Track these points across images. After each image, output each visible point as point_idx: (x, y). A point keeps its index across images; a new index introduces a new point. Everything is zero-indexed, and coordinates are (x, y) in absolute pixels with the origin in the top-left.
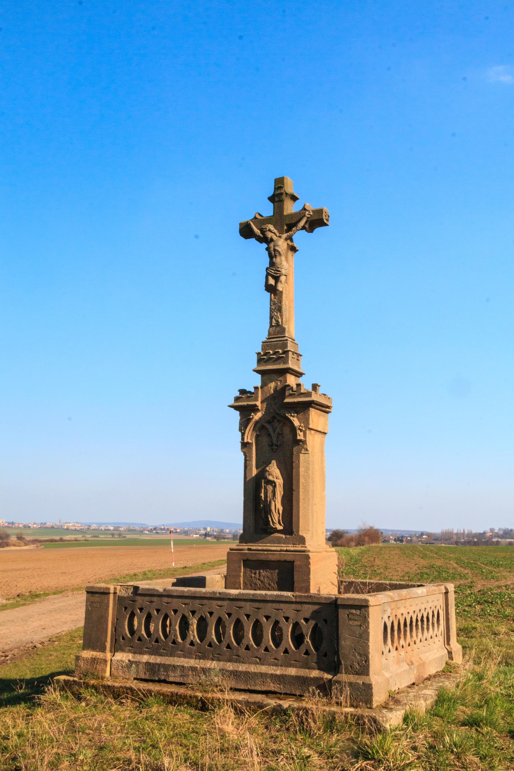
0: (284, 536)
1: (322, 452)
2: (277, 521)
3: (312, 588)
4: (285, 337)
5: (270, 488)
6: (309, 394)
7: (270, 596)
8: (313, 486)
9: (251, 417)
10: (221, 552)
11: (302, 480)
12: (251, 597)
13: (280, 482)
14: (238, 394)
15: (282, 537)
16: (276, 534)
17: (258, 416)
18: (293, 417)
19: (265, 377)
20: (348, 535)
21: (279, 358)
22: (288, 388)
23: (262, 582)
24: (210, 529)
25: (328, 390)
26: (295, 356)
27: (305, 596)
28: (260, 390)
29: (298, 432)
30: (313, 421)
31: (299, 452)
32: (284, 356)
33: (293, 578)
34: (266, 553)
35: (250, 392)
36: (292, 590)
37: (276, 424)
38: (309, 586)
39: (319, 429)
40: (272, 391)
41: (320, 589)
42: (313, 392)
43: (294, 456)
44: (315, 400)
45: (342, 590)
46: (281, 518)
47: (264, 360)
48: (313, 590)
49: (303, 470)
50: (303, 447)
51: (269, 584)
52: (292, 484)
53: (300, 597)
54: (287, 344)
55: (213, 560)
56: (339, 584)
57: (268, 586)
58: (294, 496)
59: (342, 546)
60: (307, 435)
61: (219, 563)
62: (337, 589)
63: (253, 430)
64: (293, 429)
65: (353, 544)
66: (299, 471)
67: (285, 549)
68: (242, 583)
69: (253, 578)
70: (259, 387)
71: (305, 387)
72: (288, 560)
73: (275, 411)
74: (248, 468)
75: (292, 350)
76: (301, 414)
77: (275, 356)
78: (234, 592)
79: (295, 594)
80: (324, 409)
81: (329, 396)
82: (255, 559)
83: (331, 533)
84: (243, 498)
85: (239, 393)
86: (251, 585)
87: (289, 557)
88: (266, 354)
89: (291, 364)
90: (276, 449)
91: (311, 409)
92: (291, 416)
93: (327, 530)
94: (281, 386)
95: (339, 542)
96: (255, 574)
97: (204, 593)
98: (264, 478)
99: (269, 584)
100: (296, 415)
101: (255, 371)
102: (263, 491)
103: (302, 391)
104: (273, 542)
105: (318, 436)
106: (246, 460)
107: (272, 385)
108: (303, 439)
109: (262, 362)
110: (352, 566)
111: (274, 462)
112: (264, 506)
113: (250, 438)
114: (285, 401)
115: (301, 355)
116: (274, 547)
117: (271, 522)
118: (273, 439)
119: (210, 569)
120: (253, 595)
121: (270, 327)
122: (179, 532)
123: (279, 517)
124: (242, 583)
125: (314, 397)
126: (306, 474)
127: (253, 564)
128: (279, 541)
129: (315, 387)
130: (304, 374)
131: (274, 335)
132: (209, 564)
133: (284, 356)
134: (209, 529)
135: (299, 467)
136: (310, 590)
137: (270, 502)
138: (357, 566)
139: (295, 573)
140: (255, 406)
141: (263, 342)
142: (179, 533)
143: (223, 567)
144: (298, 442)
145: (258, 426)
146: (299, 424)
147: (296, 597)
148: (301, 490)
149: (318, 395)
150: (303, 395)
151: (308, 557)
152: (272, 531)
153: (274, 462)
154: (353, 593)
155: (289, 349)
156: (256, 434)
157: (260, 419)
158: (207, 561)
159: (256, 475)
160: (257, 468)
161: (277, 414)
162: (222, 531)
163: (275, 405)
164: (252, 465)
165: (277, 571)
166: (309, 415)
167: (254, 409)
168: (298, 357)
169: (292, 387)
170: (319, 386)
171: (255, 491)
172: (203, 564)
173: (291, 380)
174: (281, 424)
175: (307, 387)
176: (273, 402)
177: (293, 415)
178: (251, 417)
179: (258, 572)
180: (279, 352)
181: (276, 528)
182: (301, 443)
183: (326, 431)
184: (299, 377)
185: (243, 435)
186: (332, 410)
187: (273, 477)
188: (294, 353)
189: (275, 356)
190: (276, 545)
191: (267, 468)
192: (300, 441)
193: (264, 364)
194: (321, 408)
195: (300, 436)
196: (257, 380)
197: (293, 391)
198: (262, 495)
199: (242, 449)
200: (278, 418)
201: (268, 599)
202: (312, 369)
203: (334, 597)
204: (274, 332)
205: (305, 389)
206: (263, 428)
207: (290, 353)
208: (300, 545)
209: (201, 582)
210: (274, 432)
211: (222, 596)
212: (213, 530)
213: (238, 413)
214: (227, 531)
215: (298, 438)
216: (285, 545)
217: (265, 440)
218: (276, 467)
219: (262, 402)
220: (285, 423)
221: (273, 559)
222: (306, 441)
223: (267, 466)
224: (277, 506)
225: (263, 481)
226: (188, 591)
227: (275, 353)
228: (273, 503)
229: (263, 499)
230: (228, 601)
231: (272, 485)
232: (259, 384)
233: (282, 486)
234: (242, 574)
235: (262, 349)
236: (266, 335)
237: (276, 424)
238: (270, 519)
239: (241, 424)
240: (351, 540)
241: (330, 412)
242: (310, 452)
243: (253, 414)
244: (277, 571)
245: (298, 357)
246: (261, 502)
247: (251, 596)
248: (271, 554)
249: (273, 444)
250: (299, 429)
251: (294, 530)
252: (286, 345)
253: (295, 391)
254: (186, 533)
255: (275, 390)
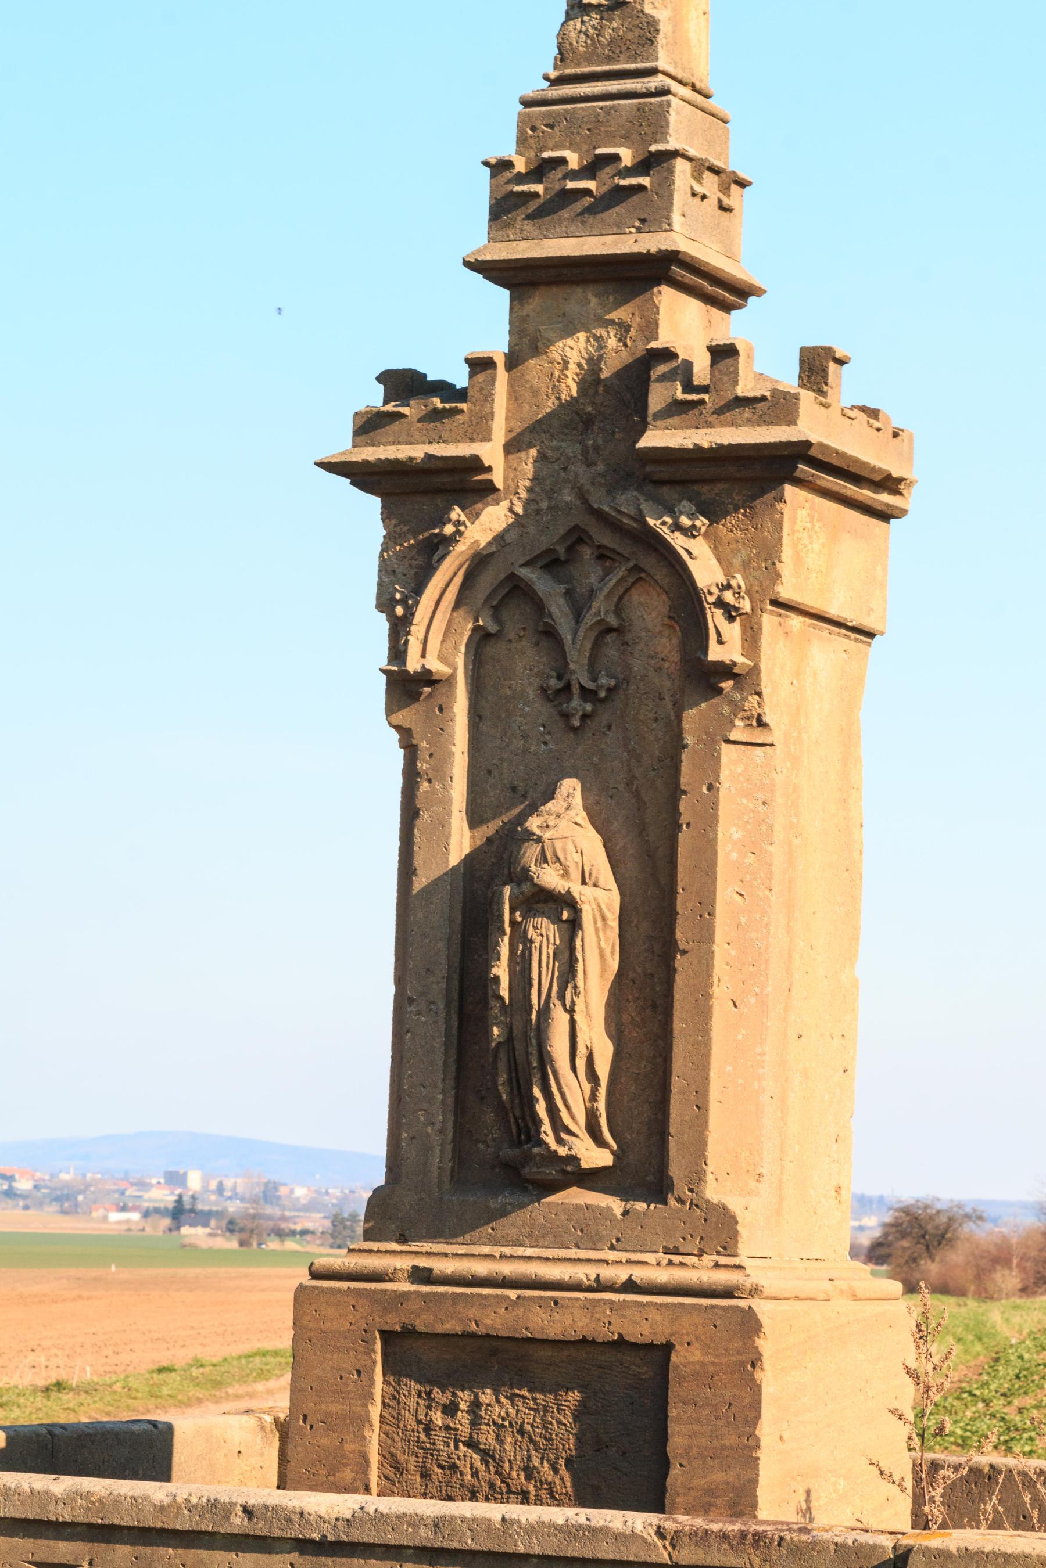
0: (616, 1205)
1: (848, 739)
2: (582, 1119)
3: (763, 1494)
4: (653, 72)
5: (544, 933)
6: (778, 406)
7: (531, 1530)
8: (789, 930)
9: (449, 529)
10: (259, 1310)
11: (725, 893)
12: (425, 1536)
13: (601, 901)
14: (374, 397)
15: (606, 1213)
16: (574, 1190)
17: (484, 526)
18: (690, 532)
19: (536, 301)
20: (981, 1233)
21: (619, 195)
22: (662, 369)
23: (486, 1455)
24: (205, 1180)
25: (895, 389)
26: (710, 184)
27: (725, 1537)
28: (502, 375)
29: (716, 618)
30: (798, 559)
31: (717, 736)
32: (645, 181)
33: (663, 1436)
34: (513, 1294)
35: (443, 389)
36: (655, 1500)
37: (588, 572)
38: (754, 1482)
39: (834, 611)
40: (571, 387)
41: (814, 1504)
42: (807, 397)
43: (685, 756)
44: (814, 438)
45: (935, 1511)
46: (601, 1106)
47: (533, 206)
48: (773, 1507)
49: (736, 836)
50: (737, 708)
51: (529, 1471)
52: (671, 914)
53: (702, 1538)
54: (662, 114)
55: (213, 1352)
56: (917, 1480)
57: (519, 1479)
58: (679, 980)
59: (943, 1289)
60: (765, 640)
61: (253, 1366)
62: (904, 1504)
63: (458, 604)
64: (688, 607)
65: (1009, 1279)
66: (711, 845)
67: (621, 1274)
68: (374, 1459)
69: (439, 1436)
70: (500, 361)
71: (758, 368)
72: (639, 1340)
73: (582, 495)
74: (425, 817)
75: (692, 152)
76: (731, 520)
77: (591, 185)
78: (326, 1506)
79: (669, 1525)
80: (869, 491)
81: (896, 423)
82: (451, 1326)
83: (888, 1218)
84: (389, 990)
85: (380, 388)
86: (425, 1475)
87: (643, 1322)
88: (540, 170)
89: (687, 231)
90: (585, 717)
91: (789, 490)
92: (677, 527)
93: (863, 1203)
94: (625, 357)
95: (932, 1268)
96: (450, 1410)
97: (161, 1509)
98: (510, 880)
99: (529, 1471)
100: (701, 522)
101: (475, 266)
102: (504, 949)
103: (741, 391)
104: (552, 1235)
105: (826, 650)
106: (411, 776)
107: (575, 349)
108: (739, 659)
109: (520, 215)
110: (998, 1404)
111: (570, 787)
112: (510, 1029)
113: (440, 644)
114: (642, 444)
115: (743, 184)
116: (559, 1265)
117: (546, 1126)
118: (572, 654)
119: (200, 1401)
120: (437, 1524)
121: (569, 17)
122: (24, 1196)
123: (594, 1097)
124: (374, 1459)
125: (813, 425)
126: (750, 859)
127: (436, 1357)
128: (587, 1232)
129: (817, 366)
130: (757, 291)
131: (589, 60)
132: (195, 1372)
133: (645, 181)
134: (194, 1182)
135: (711, 820)
136: (754, 1506)
137: (545, 1012)
138: (1029, 1401)
139: (673, 1413)
140: (475, 464)
141: (527, 103)
142: (29, 1201)
143: (270, 1392)
144: (708, 678)
145: (487, 581)
146: (721, 579)
147: (675, 1540)
148: (719, 948)
149: (835, 412)
150: (747, 413)
151: (749, 1325)
152: (552, 1173)
153: (570, 787)
154: (996, 1524)
155: (672, 144)
156: (476, 629)
157: (500, 539)
158: (181, 1357)
159: (470, 860)
160: (475, 819)
161: (599, 515)
162: (270, 1193)
163: (589, 464)
164: (446, 802)
165: (574, 1397)
166: (779, 526)
167: (466, 482)
168: (725, 189)
169: (688, 365)
170: (841, 362)
171: (459, 943)
172: (161, 1370)
173: (682, 324)
174: (621, 572)
175: (769, 362)
176: (572, 449)
177: (685, 521)
178: (449, 529)
179: (464, 1398)
180: (616, 158)
181: (574, 1159)
182: (727, 685)
183: (868, 622)
184: (727, 308)
185: (399, 629)
186: (912, 500)
187: (566, 875)
188: (702, 167)
189: (591, 185)
190: (573, 1253)
191: (534, 823)
192: (726, 670)
193: (529, 227)
194: (850, 489)
195: (726, 645)
196: (486, 319)
197: (689, 387)
198: (501, 970)
199: (390, 710)
200: (606, 539)
201: (521, 1549)
202: (813, 262)
203: (887, 1542)
204: (594, 42)
205: (760, 377)
206: (514, 589)
207: (681, 166)
208: (708, 1259)
209: (145, 1451)
210: (578, 617)
211: (260, 1528)
212: (220, 1189)
213: (374, 503)
214: (300, 1192)
215: (715, 653)
216: (623, 1256)
217: (524, 665)
218: (582, 817)
219: (512, 447)
220: (637, 568)
221: (554, 1332)
222: (755, 670)
223: (533, 809)
224: (583, 1033)
225: (507, 891)
226: (68, 1500)
227: (593, 167)
228: (560, 1020)
229: (504, 992)
230: (294, 1557)
231: (557, 920)
232: (497, 343)
233: (615, 924)
234: (375, 1411)
235: (522, 141)
236: (544, 60)
237: (588, 572)
238: (541, 1108)
239: (386, 569)
240: (999, 1257)
241: (902, 513)
242: (776, 734)
243: (456, 513)
244: (574, 1397)
245: (725, 189)
246: (496, 1010)
247: (423, 1531)
248: (541, 1302)
249: (568, 687)
250: (720, 603)
251: (675, 1171)
252: (656, 123)
253: (705, 389)
254: (65, 1199)
255: (590, 381)
